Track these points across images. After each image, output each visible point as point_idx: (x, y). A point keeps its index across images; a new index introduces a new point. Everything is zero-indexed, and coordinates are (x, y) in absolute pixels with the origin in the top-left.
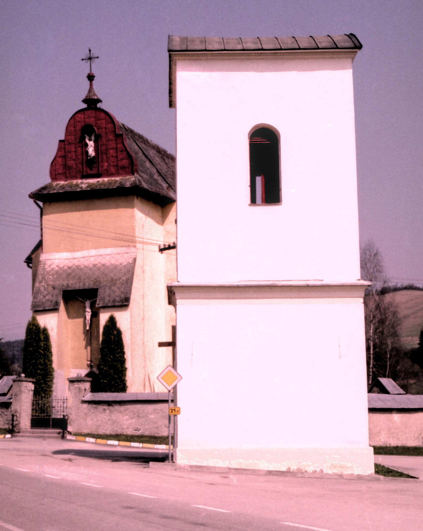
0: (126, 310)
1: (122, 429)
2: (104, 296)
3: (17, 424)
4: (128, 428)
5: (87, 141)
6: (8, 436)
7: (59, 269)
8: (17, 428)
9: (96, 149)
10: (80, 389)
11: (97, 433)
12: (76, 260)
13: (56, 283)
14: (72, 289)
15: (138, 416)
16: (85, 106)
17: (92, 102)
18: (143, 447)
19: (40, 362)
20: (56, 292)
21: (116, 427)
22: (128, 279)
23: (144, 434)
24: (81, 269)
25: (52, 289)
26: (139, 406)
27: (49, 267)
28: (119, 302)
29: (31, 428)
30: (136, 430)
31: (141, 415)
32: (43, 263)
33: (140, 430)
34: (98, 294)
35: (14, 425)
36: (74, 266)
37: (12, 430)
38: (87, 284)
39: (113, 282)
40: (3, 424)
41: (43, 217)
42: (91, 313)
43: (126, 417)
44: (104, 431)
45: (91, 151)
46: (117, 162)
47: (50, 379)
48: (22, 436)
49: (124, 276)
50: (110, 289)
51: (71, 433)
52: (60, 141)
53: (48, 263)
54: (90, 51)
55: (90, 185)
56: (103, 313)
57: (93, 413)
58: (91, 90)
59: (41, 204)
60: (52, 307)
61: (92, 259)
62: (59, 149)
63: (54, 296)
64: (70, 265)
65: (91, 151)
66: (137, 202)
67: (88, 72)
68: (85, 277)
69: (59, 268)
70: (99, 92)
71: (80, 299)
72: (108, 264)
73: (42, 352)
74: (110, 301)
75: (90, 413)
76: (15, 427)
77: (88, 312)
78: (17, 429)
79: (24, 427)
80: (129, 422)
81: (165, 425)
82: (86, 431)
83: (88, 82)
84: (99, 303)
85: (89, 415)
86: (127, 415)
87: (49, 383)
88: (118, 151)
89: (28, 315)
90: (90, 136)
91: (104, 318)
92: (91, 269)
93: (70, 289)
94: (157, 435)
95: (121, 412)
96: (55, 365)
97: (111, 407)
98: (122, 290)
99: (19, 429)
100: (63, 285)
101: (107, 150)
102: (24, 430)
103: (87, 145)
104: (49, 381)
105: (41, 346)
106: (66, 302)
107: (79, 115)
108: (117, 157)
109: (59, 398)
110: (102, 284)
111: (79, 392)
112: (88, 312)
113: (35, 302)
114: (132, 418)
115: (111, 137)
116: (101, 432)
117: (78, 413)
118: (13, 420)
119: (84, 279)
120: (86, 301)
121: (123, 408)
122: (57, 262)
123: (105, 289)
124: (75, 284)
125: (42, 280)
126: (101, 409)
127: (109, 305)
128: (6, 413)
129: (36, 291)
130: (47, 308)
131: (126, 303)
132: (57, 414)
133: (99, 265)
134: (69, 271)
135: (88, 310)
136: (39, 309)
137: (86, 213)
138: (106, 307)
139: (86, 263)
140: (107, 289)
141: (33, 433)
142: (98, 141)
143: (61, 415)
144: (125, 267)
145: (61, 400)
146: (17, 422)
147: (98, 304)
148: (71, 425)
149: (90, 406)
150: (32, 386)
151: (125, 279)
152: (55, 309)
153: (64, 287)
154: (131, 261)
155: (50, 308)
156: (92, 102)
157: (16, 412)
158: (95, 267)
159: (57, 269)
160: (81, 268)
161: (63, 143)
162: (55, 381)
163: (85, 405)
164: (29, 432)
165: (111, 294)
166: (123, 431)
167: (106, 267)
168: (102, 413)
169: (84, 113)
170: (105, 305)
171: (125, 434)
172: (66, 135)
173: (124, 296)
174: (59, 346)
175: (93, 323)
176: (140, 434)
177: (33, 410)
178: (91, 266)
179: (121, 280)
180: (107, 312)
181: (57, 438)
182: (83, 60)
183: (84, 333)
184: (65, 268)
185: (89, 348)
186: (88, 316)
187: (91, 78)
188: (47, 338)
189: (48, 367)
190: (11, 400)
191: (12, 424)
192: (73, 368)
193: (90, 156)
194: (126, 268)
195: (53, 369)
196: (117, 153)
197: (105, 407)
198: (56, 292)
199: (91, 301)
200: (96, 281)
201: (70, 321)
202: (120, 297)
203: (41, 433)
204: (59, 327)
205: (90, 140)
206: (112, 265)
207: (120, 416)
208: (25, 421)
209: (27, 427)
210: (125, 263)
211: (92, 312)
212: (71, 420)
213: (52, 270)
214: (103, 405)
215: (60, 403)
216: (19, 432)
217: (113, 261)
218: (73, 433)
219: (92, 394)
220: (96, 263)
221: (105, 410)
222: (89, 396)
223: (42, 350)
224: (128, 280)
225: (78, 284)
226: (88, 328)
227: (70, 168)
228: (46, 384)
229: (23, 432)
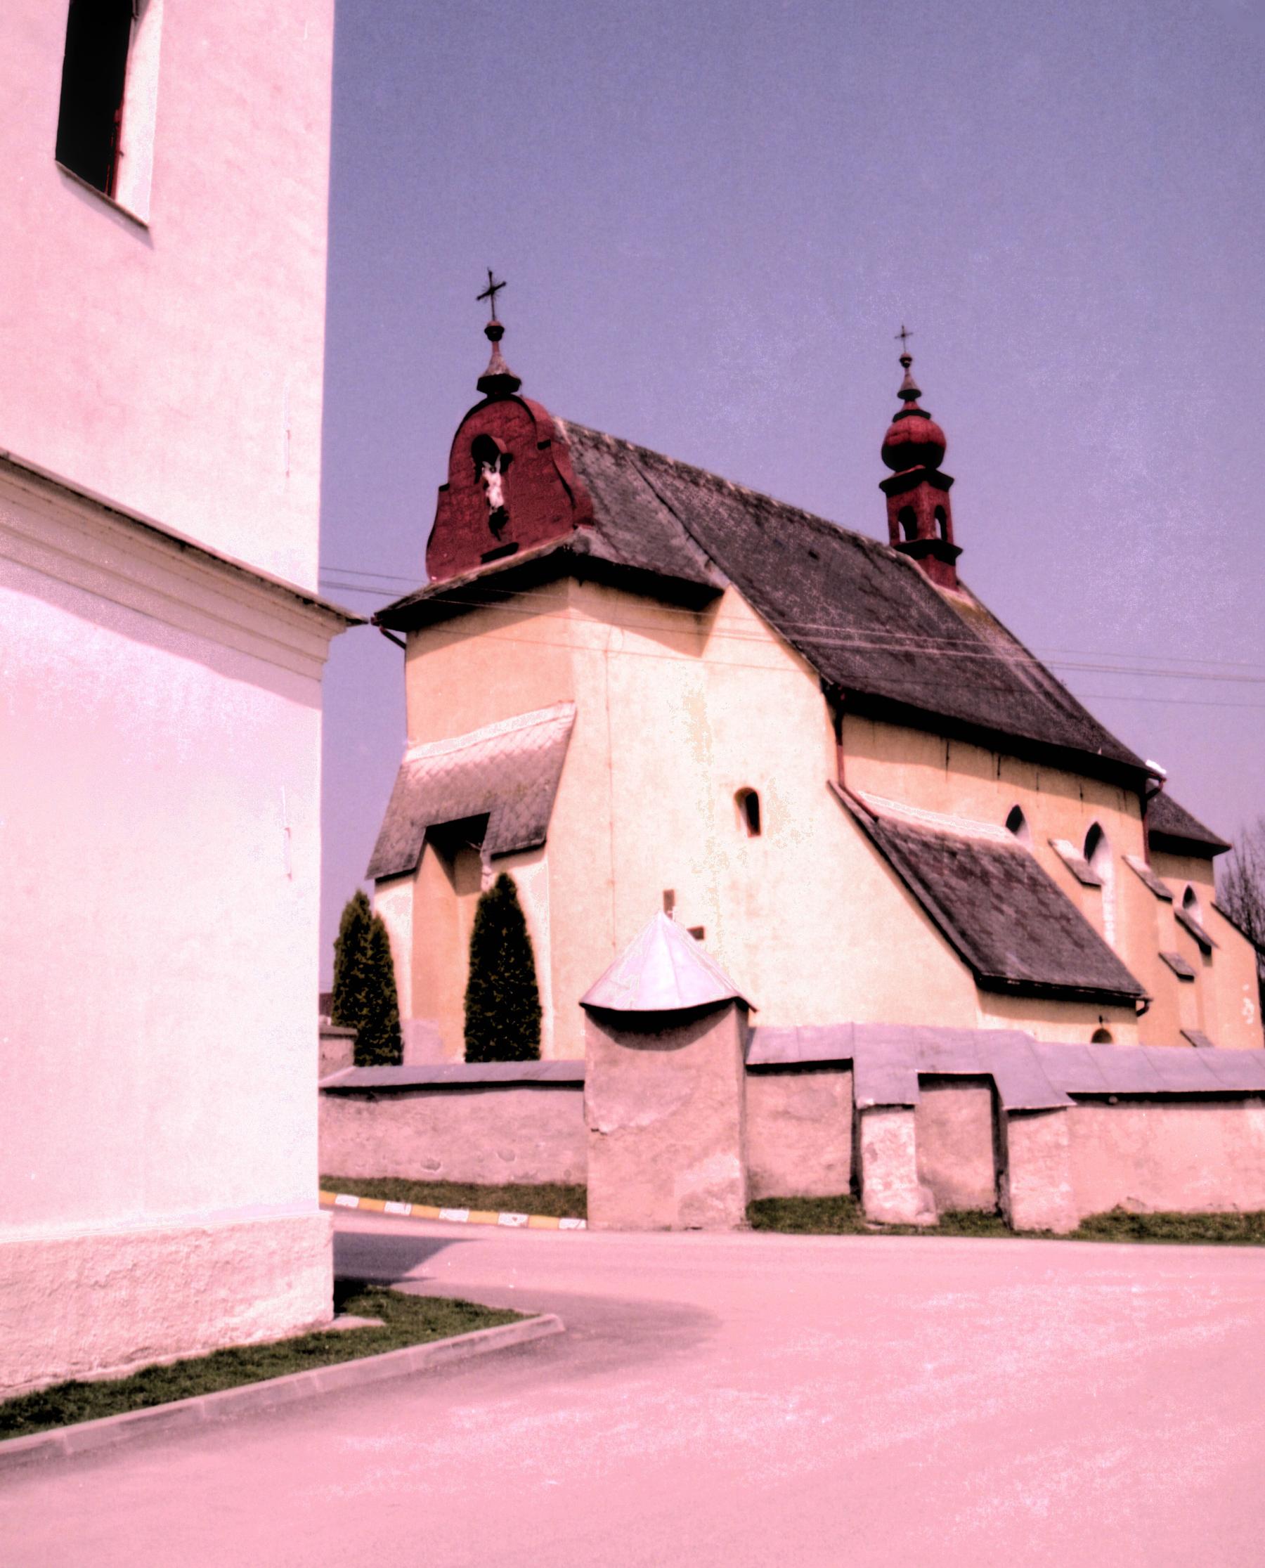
0: (539, 860)
1: (398, 1163)
2: (502, 830)
15: (434, 1129)
16: (483, 396)
17: (499, 388)
18: (411, 1218)
30: (429, 1167)
33: (439, 1165)
38: (471, 806)
39: (520, 791)
43: (408, 1131)
45: (496, 496)
54: (490, 274)
59: (402, 636)
61: (491, 744)
65: (496, 496)
66: (572, 589)
67: (486, 320)
81: (500, 1155)
86: (407, 1124)
94: (479, 1181)
95: (394, 1118)
97: (372, 1105)
110: (499, 801)
114: (419, 1133)
126: (352, 1110)
131: (538, 841)
134: (447, 780)
140: (507, 810)
144: (547, 753)
152: (409, 872)
156: (499, 388)
166: (399, 1168)
172: (451, 474)
174: (419, 962)
176: (440, 1178)
184: (442, 774)
200: (491, 796)
205: (493, 470)
214: (356, 1100)
219: (353, 1068)
221: (359, 1112)
222: (349, 1074)
223: (362, 971)
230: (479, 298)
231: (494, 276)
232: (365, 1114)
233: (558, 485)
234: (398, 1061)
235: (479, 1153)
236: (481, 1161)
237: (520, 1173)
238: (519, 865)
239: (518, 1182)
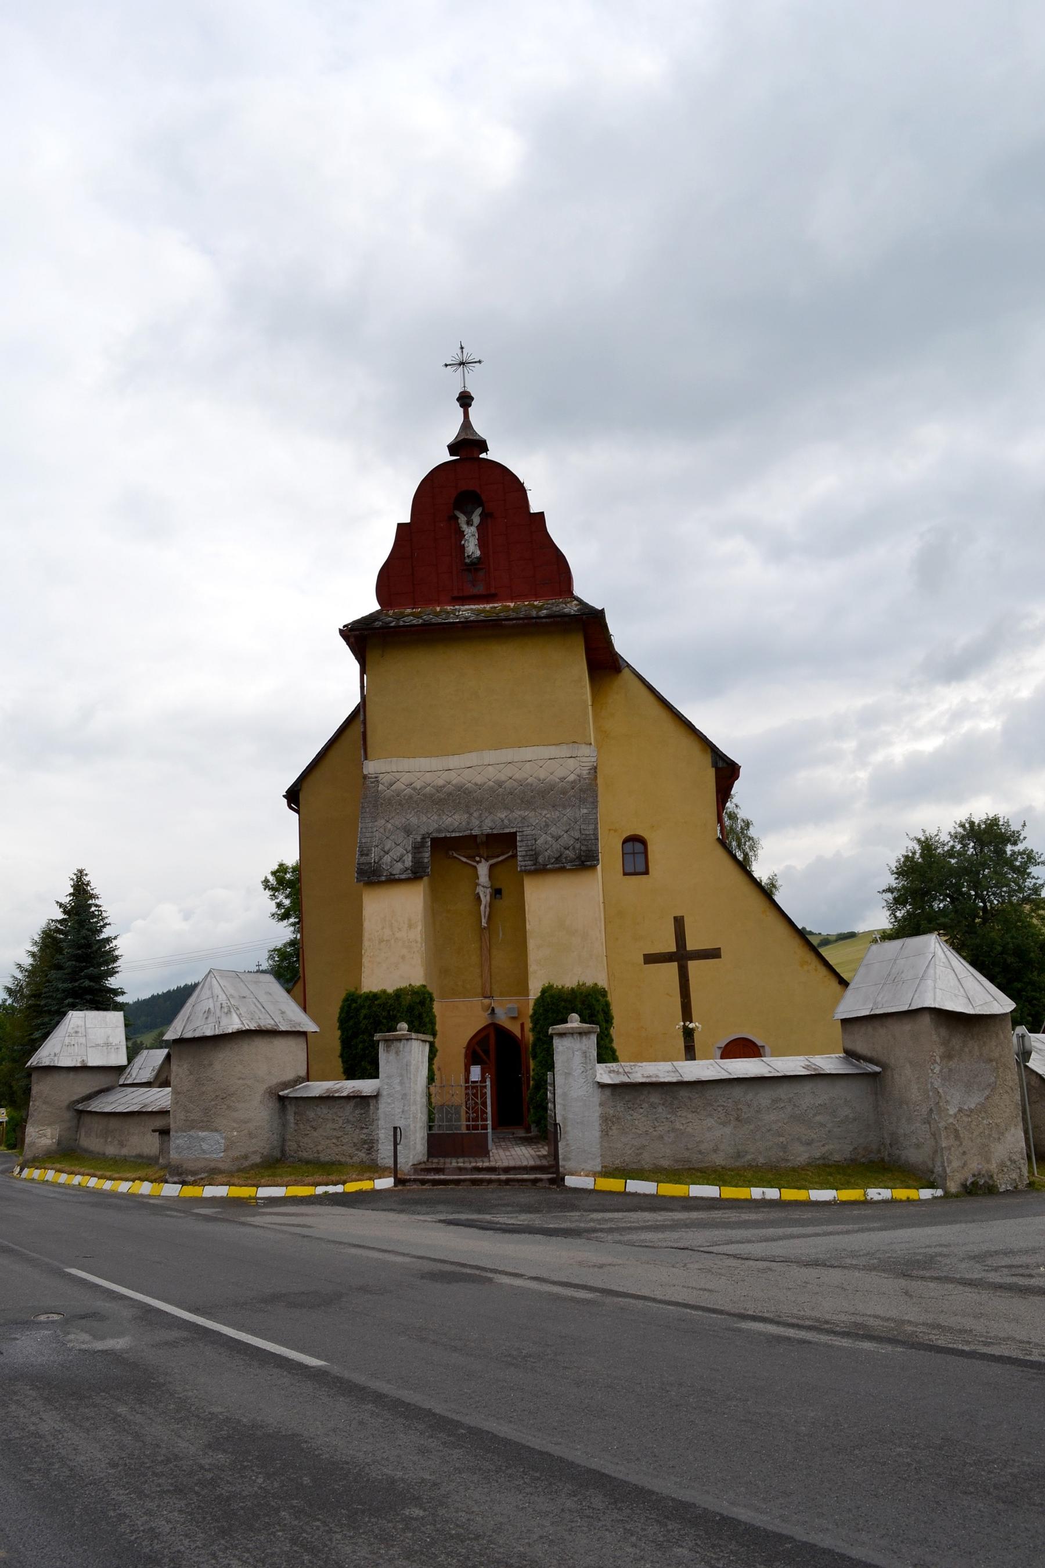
4: (715, 1150)
5: (464, 527)
9: (482, 544)
12: (453, 774)
15: (737, 1119)
17: (468, 446)
43: (710, 1122)
45: (472, 547)
53: (385, 779)
55: (479, 612)
58: (467, 425)
69: (414, 789)
70: (481, 428)
83: (462, 410)
86: (711, 1115)
90: (469, 514)
103: (461, 534)
122: (406, 778)
124: (453, 822)
139: (479, 780)
156: (468, 446)
159: (408, 791)
182: (446, 365)
187: (465, 400)
205: (469, 523)
210: (572, 777)
226: (484, 924)
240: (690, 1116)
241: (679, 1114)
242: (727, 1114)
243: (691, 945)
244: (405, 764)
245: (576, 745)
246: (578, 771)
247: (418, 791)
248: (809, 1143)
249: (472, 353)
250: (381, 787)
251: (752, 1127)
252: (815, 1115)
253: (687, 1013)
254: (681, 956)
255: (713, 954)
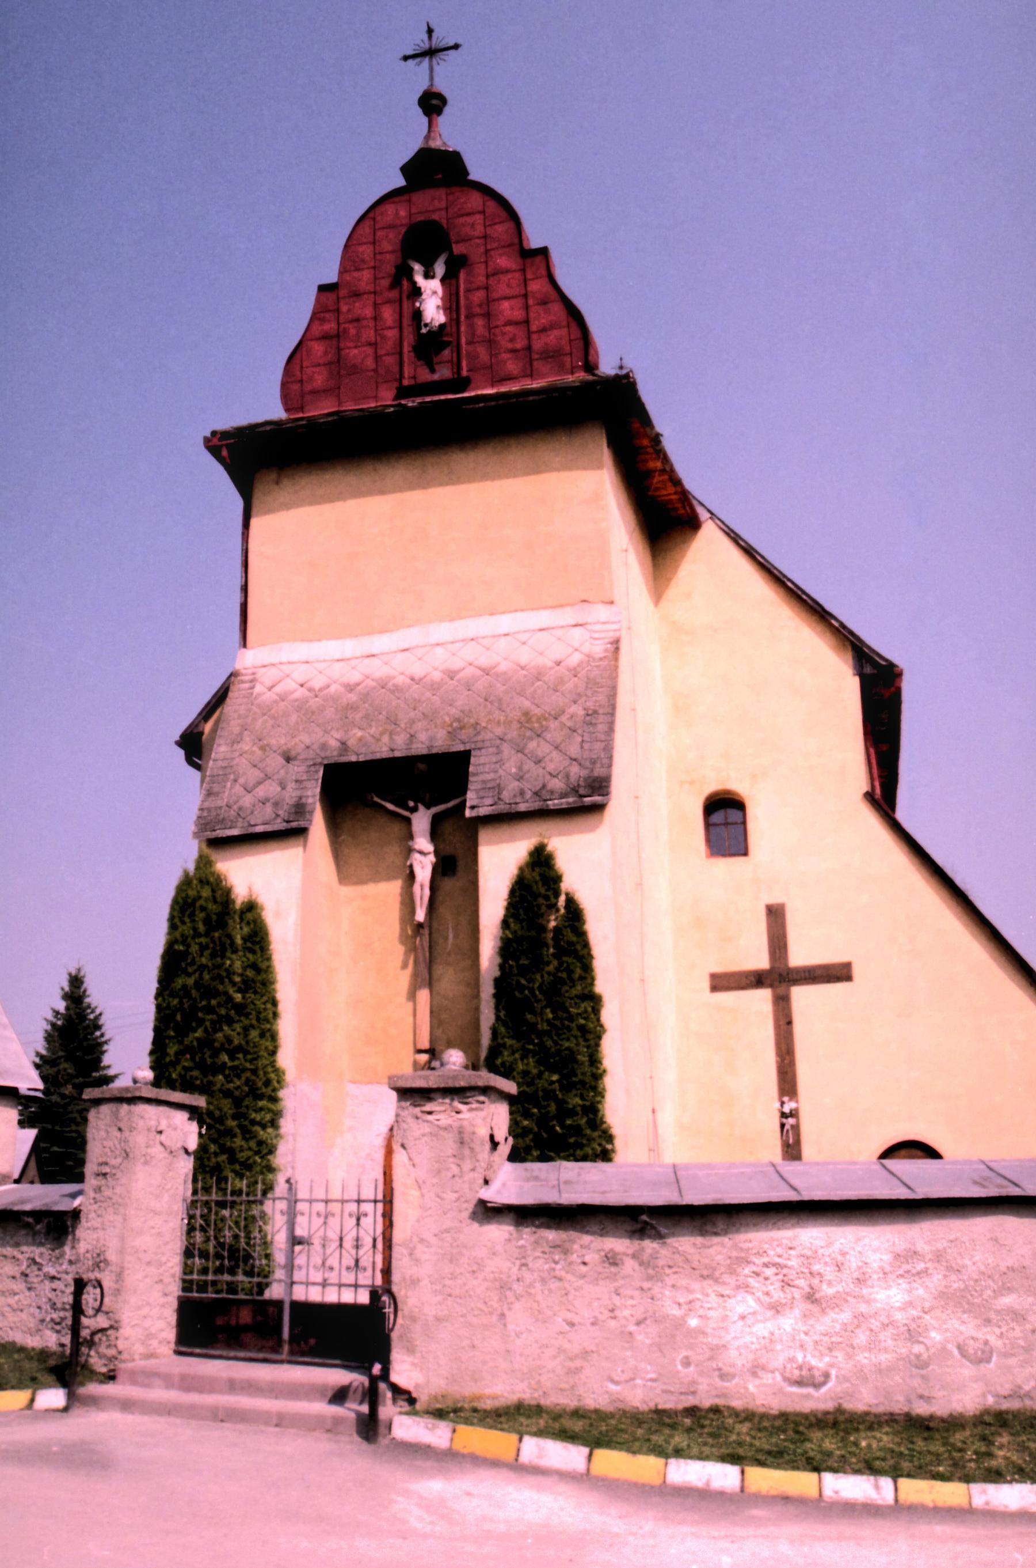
1: (724, 1376)
3: (103, 1330)
5: (419, 279)
6: (53, 1397)
7: (307, 693)
8: (103, 1349)
9: (451, 304)
10: (463, 1139)
11: (569, 1402)
12: (376, 662)
13: (297, 740)
14: (362, 759)
15: (811, 1297)
17: (435, 169)
19: (229, 1040)
20: (297, 769)
21: (687, 1363)
22: (595, 712)
23: (848, 1406)
24: (397, 690)
25: (281, 761)
26: (811, 1236)
27: (270, 689)
28: (563, 796)
29: (178, 1353)
30: (800, 1383)
31: (827, 1290)
32: (250, 677)
34: (471, 769)
35: (85, 1333)
36: (369, 682)
37: (70, 1367)
38: (423, 737)
39: (531, 725)
40: (32, 1324)
41: (255, 522)
42: (432, 858)
43: (745, 1304)
44: (612, 1387)
45: (433, 309)
46: (529, 338)
47: (268, 1117)
48: (127, 1405)
49: (575, 702)
50: (520, 751)
51: (412, 1401)
52: (323, 289)
53: (267, 676)
56: (489, 844)
57: (543, 1281)
60: (279, 825)
62: (316, 316)
63: (291, 785)
64: (354, 677)
65: (433, 309)
68: (412, 714)
69: (310, 690)
71: (390, 807)
72: (503, 667)
73: (238, 997)
74: (522, 793)
75: (528, 1277)
76: (91, 1343)
77: (421, 852)
78: (101, 1356)
79: (139, 1348)
80: (762, 1329)
82: (502, 1389)
84: (477, 801)
85: (518, 1288)
86: (746, 1288)
87: (262, 1134)
88: (531, 302)
89: (184, 854)
91: (500, 862)
92: (434, 687)
93: (353, 758)
94: (921, 1409)
95: (709, 1275)
96: (286, 1058)
97: (649, 1245)
98: (574, 750)
99: (112, 1359)
100: (324, 746)
101: (489, 301)
102: (141, 1363)
103: (416, 292)
104: (264, 1127)
105: (230, 973)
106: (334, 825)
107: (390, 209)
108: (527, 322)
109: (336, 1193)
111: (459, 1157)
112: (421, 852)
113: (209, 810)
114: (777, 1308)
115: (504, 261)
116: (597, 1392)
117: (453, 1277)
118: (77, 1309)
119: (412, 722)
120: (414, 810)
121: (718, 1248)
122: (300, 674)
123: (499, 752)
125: (241, 734)
127: (523, 807)
128: (51, 1270)
129: (215, 772)
130: (260, 829)
131: (597, 799)
132: (320, 1276)
133: (470, 671)
135: (423, 842)
136: (222, 839)
137: (416, 496)
138: (507, 819)
139: (418, 670)
141: (188, 1384)
142: (457, 278)
143: (356, 1286)
144: (574, 672)
145: (343, 1202)
146: (102, 1321)
147: (473, 807)
148: (411, 1350)
149: (528, 1235)
150: (188, 1133)
151: (582, 712)
152: (293, 833)
153: (328, 753)
154: (599, 649)
155: (269, 828)
156: (435, 169)
157: (100, 1262)
158: (452, 679)
159: (301, 693)
160: (395, 686)
161: (331, 297)
162: (286, 1125)
163: (499, 1232)
164: (168, 1381)
165: (526, 767)
167: (497, 675)
168: (595, 1282)
169: (410, 201)
170: (502, 808)
171: (737, 1404)
172: (343, 271)
173: (584, 773)
175: (440, 898)
176: (829, 1406)
177: (188, 1253)
178: (437, 676)
179: (564, 719)
180: (512, 839)
181: (332, 1427)
183: (404, 939)
185: (424, 996)
186: (424, 868)
187: (432, 104)
188: (258, 939)
189: (260, 1063)
190: (76, 1203)
191: (76, 1328)
192: (354, 1082)
193: (426, 325)
194: (583, 673)
195: (279, 1073)
196: (527, 307)
197: (619, 1244)
198: (297, 769)
199: (435, 810)
201: (348, 891)
202: (568, 776)
203: (233, 1386)
204: (307, 911)
205: (428, 275)
206: (523, 668)
207: (707, 1296)
208: (145, 1311)
209: (154, 1343)
210: (575, 659)
211: (436, 852)
212: (414, 1319)
213: (282, 698)
214: (603, 1233)
215: (334, 1223)
216: (111, 1377)
217: (525, 656)
218: (423, 1399)
220: (456, 664)
221: (612, 1260)
222: (512, 1183)
224: (591, 714)
225: (385, 739)
226: (420, 916)
227: (355, 370)
228: (247, 1133)
229: (134, 1377)
230: (406, 58)
231: (434, 35)
232: (630, 1265)
233: (557, 309)
234: (605, 1156)
235: (917, 1349)
236: (924, 1365)
237: (1006, 1389)
238: (560, 834)
239: (1005, 1406)
240: (696, 1286)
241: (669, 1281)
242: (786, 1284)
243: (761, 961)
244: (301, 651)
245: (585, 605)
246: (586, 648)
247: (315, 693)
248: (983, 1357)
249: (444, 36)
250: (258, 688)
251: (845, 1316)
252: (998, 1293)
253: (787, 1082)
254: (779, 978)
255: (838, 973)
